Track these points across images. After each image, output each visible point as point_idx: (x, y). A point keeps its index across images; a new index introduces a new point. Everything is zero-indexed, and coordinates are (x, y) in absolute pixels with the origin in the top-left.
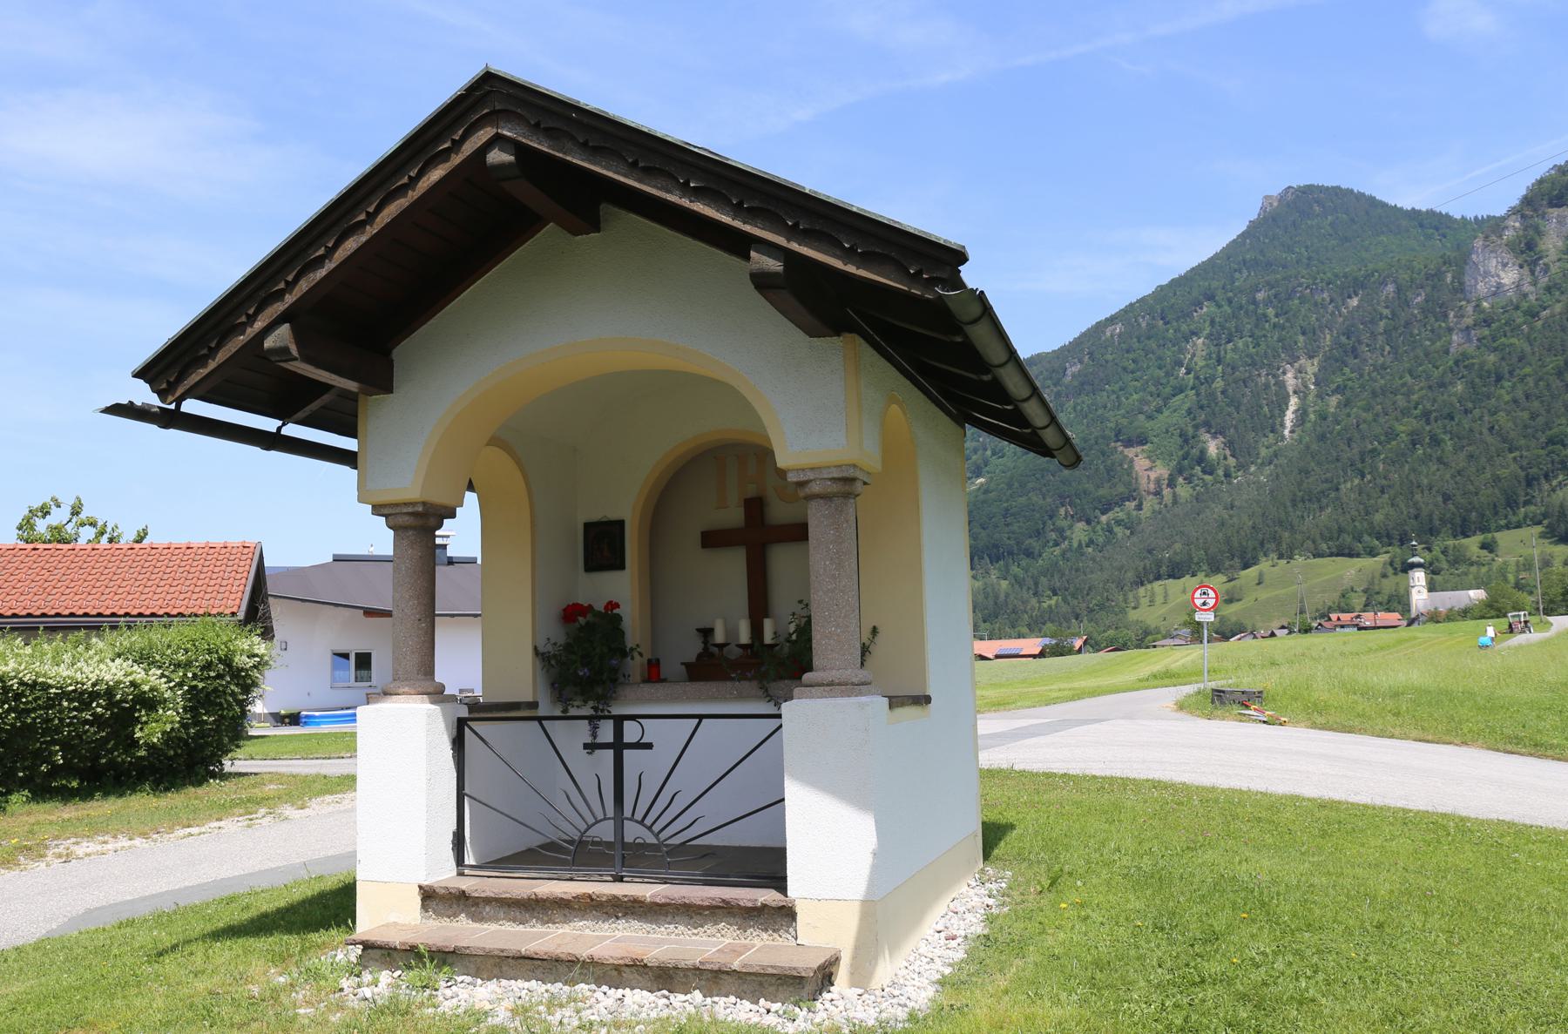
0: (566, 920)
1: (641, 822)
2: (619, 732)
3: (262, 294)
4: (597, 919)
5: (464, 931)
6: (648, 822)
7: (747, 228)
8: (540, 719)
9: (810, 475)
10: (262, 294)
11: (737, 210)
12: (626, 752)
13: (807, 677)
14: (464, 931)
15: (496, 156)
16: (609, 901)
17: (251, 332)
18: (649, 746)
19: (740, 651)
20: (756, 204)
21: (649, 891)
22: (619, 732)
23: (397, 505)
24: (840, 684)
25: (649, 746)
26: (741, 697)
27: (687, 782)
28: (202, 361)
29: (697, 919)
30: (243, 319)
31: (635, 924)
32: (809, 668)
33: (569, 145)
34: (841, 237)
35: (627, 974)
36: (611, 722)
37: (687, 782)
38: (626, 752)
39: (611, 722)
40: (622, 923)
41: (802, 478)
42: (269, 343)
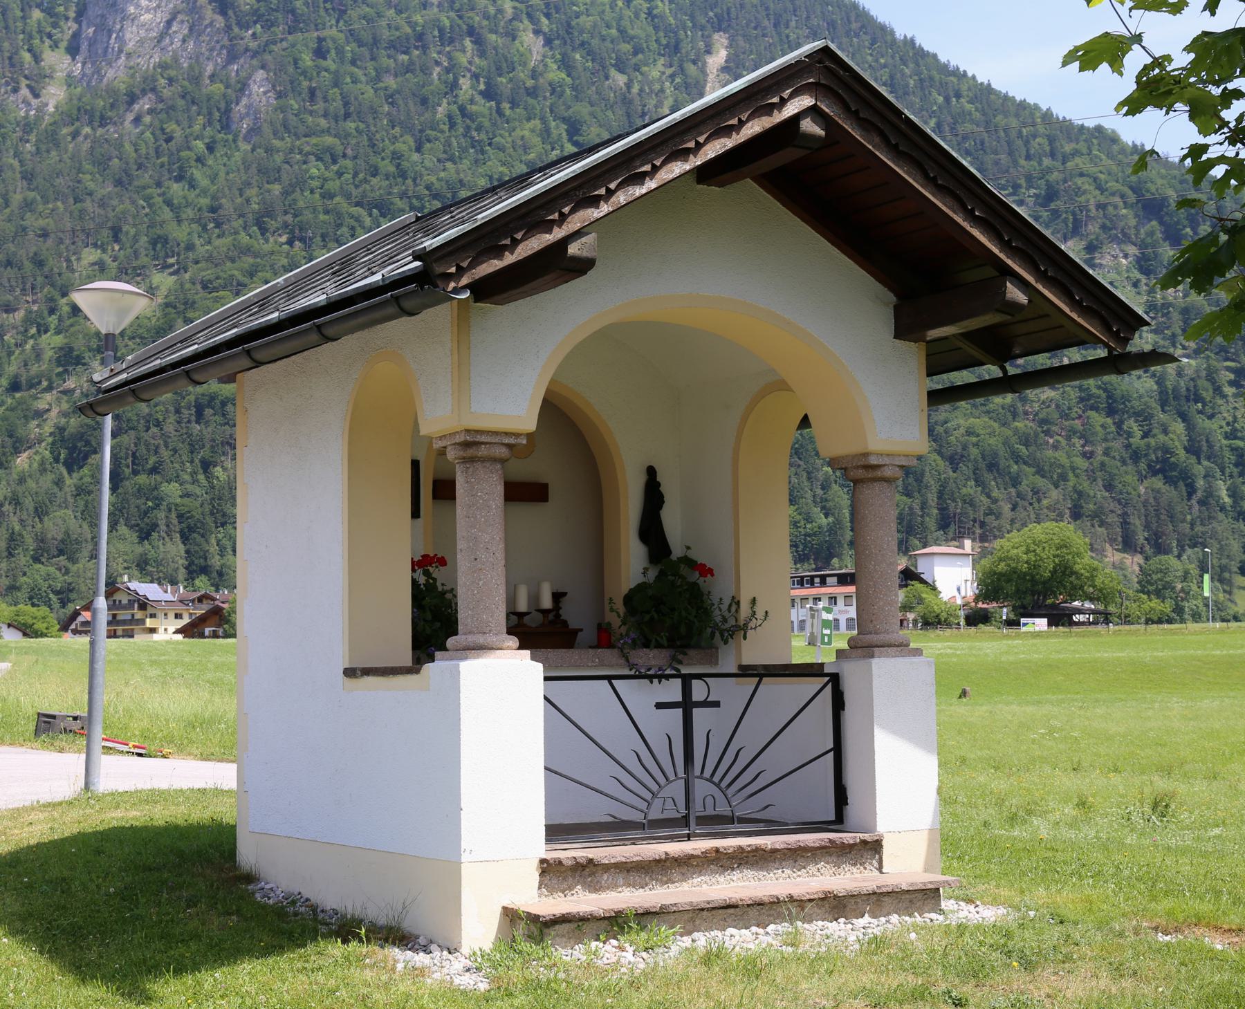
0: (685, 877)
1: (710, 780)
2: (687, 691)
3: (580, 194)
4: (713, 872)
5: (581, 901)
6: (716, 779)
7: (1009, 262)
8: (609, 678)
9: (886, 461)
10: (580, 194)
11: (1006, 246)
12: (696, 712)
13: (450, 642)
14: (581, 901)
15: (808, 126)
16: (753, 851)
17: (558, 234)
18: (716, 704)
19: (540, 616)
20: (1020, 245)
21: (675, 848)
22: (687, 691)
23: (496, 433)
24: (895, 646)
25: (716, 704)
26: (602, 665)
27: (749, 740)
28: (498, 252)
29: (801, 862)
30: (556, 216)
31: (749, 873)
32: (455, 633)
33: (877, 140)
34: (1074, 290)
35: (851, 905)
36: (679, 680)
37: (749, 740)
38: (696, 712)
39: (679, 680)
40: (736, 875)
41: (881, 462)
42: (573, 249)
